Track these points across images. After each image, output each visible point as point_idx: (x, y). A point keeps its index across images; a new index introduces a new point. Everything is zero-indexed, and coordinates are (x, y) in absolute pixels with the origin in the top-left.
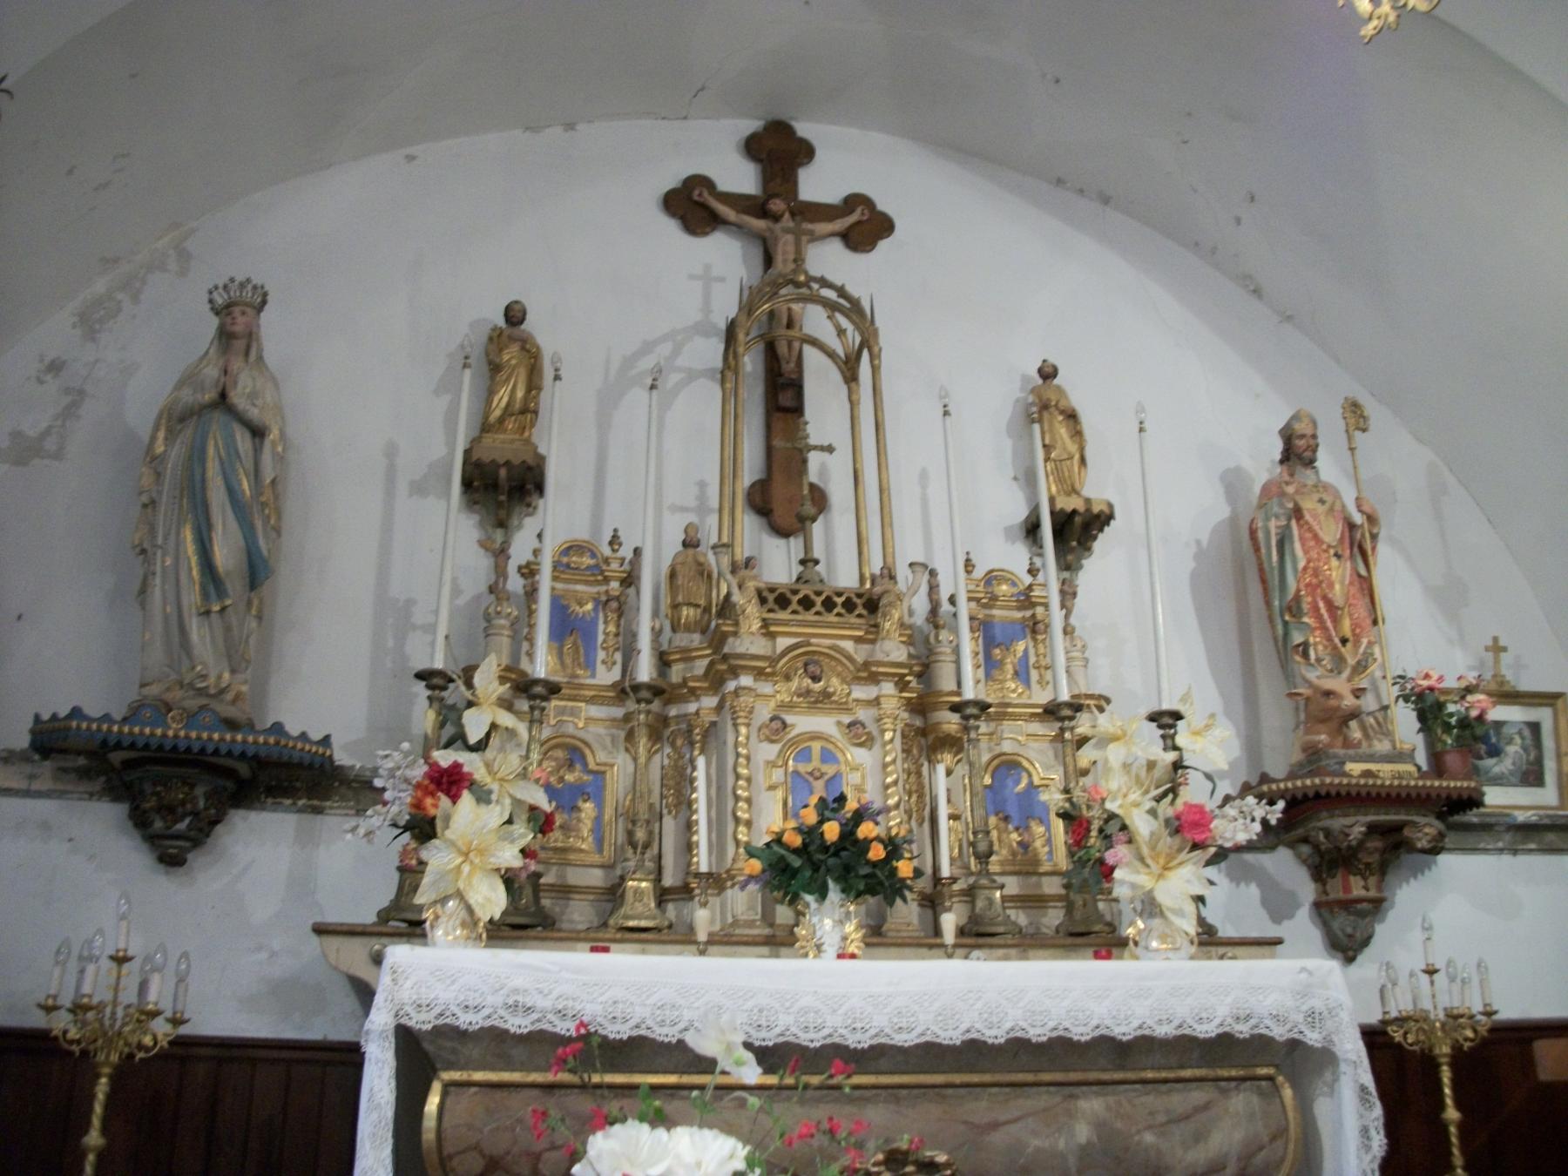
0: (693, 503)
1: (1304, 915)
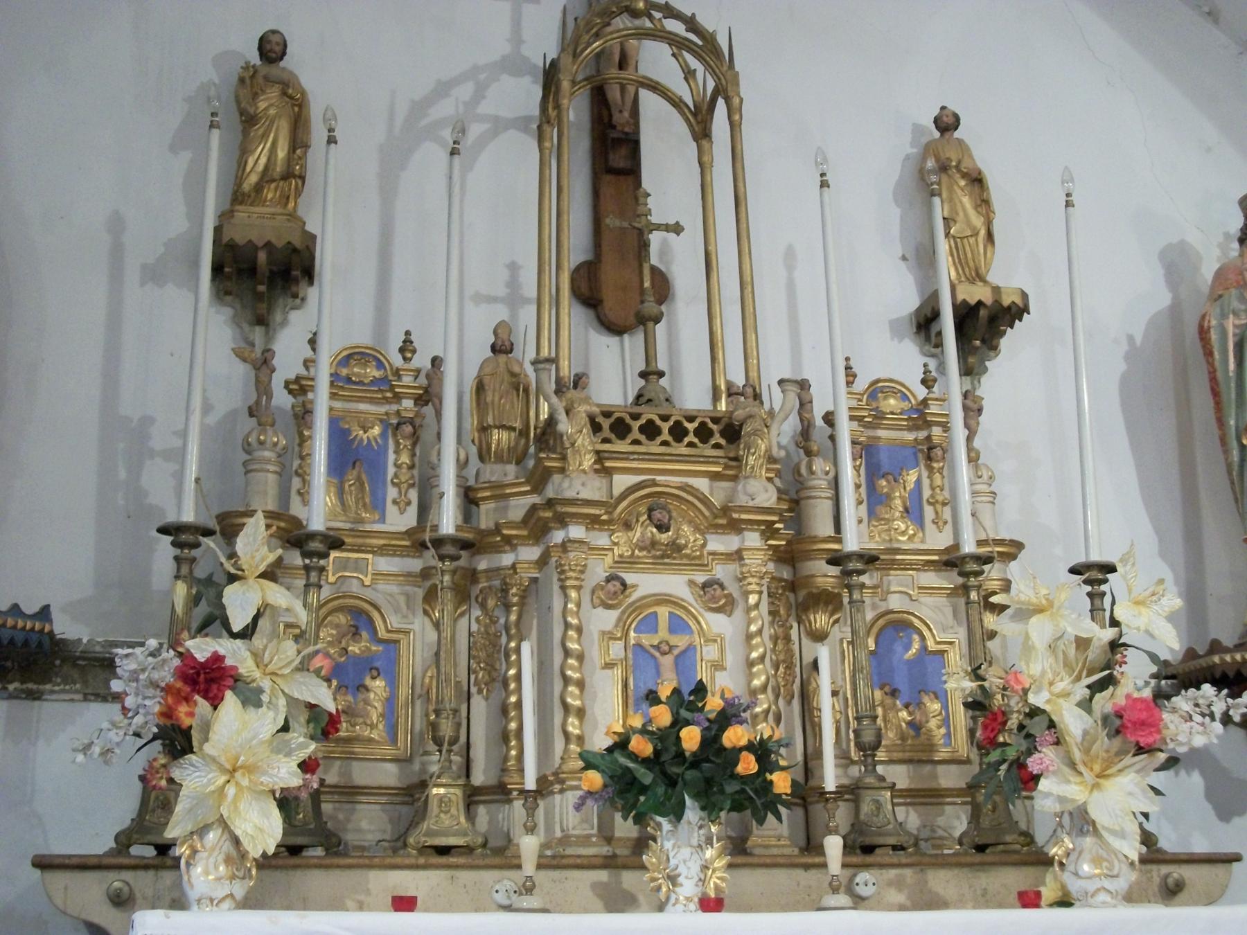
0: (502, 291)
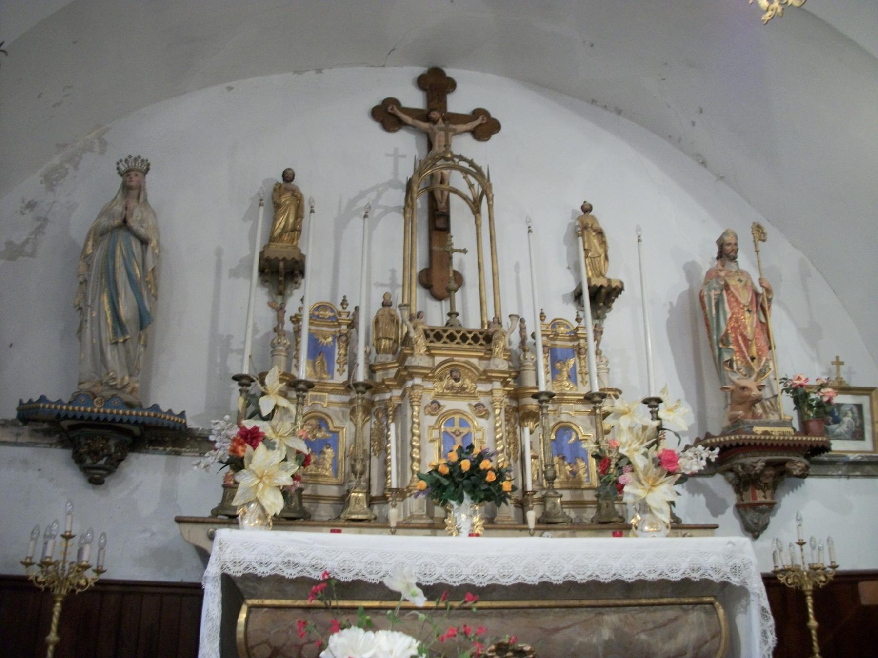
0: (388, 281)
1: (730, 512)
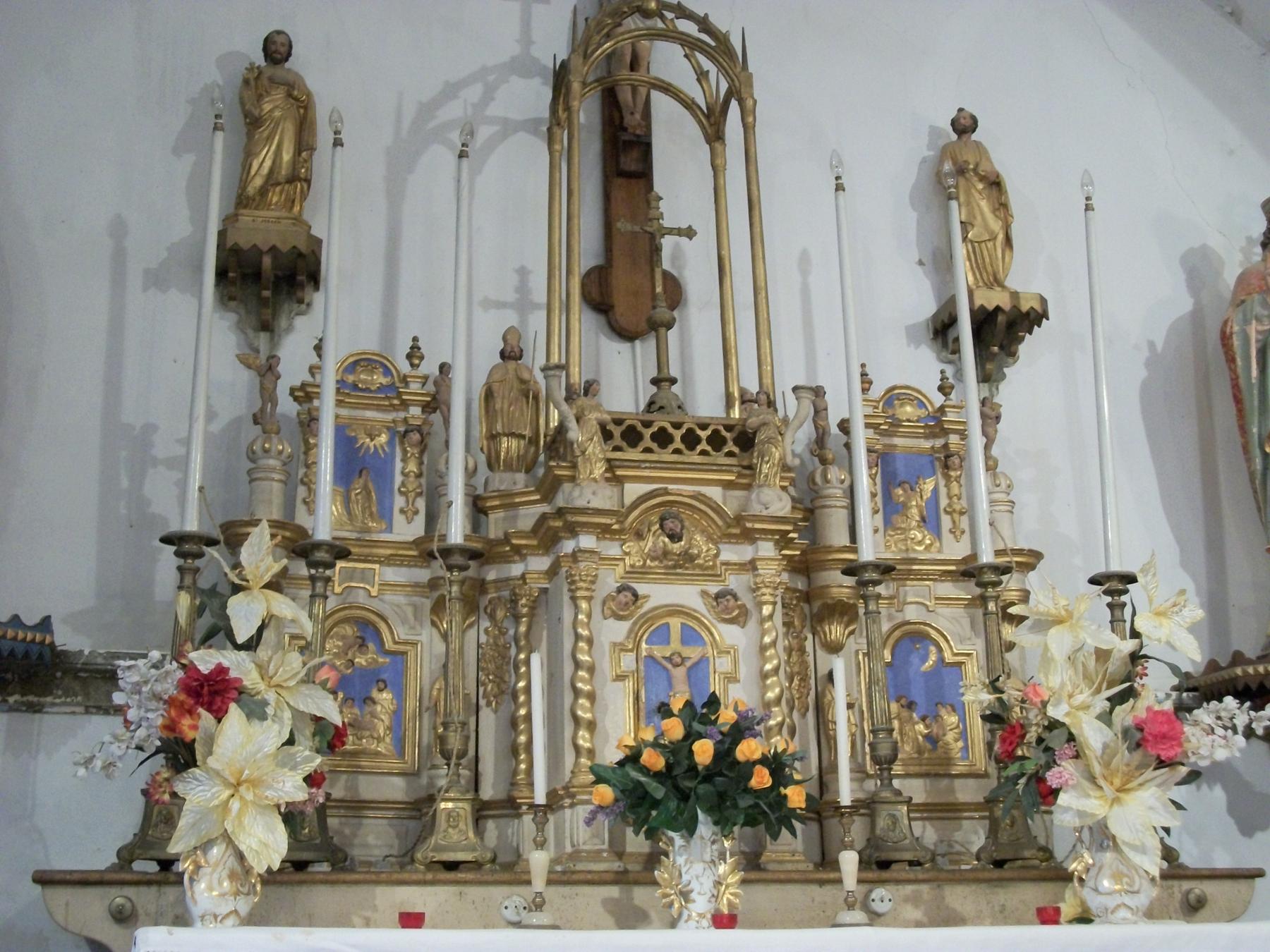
0: (511, 296)
